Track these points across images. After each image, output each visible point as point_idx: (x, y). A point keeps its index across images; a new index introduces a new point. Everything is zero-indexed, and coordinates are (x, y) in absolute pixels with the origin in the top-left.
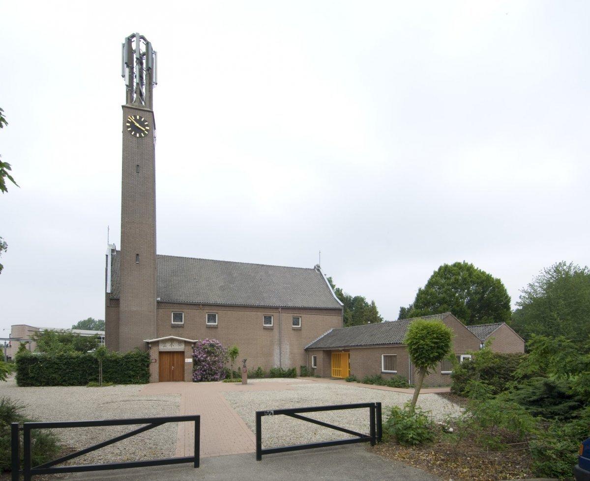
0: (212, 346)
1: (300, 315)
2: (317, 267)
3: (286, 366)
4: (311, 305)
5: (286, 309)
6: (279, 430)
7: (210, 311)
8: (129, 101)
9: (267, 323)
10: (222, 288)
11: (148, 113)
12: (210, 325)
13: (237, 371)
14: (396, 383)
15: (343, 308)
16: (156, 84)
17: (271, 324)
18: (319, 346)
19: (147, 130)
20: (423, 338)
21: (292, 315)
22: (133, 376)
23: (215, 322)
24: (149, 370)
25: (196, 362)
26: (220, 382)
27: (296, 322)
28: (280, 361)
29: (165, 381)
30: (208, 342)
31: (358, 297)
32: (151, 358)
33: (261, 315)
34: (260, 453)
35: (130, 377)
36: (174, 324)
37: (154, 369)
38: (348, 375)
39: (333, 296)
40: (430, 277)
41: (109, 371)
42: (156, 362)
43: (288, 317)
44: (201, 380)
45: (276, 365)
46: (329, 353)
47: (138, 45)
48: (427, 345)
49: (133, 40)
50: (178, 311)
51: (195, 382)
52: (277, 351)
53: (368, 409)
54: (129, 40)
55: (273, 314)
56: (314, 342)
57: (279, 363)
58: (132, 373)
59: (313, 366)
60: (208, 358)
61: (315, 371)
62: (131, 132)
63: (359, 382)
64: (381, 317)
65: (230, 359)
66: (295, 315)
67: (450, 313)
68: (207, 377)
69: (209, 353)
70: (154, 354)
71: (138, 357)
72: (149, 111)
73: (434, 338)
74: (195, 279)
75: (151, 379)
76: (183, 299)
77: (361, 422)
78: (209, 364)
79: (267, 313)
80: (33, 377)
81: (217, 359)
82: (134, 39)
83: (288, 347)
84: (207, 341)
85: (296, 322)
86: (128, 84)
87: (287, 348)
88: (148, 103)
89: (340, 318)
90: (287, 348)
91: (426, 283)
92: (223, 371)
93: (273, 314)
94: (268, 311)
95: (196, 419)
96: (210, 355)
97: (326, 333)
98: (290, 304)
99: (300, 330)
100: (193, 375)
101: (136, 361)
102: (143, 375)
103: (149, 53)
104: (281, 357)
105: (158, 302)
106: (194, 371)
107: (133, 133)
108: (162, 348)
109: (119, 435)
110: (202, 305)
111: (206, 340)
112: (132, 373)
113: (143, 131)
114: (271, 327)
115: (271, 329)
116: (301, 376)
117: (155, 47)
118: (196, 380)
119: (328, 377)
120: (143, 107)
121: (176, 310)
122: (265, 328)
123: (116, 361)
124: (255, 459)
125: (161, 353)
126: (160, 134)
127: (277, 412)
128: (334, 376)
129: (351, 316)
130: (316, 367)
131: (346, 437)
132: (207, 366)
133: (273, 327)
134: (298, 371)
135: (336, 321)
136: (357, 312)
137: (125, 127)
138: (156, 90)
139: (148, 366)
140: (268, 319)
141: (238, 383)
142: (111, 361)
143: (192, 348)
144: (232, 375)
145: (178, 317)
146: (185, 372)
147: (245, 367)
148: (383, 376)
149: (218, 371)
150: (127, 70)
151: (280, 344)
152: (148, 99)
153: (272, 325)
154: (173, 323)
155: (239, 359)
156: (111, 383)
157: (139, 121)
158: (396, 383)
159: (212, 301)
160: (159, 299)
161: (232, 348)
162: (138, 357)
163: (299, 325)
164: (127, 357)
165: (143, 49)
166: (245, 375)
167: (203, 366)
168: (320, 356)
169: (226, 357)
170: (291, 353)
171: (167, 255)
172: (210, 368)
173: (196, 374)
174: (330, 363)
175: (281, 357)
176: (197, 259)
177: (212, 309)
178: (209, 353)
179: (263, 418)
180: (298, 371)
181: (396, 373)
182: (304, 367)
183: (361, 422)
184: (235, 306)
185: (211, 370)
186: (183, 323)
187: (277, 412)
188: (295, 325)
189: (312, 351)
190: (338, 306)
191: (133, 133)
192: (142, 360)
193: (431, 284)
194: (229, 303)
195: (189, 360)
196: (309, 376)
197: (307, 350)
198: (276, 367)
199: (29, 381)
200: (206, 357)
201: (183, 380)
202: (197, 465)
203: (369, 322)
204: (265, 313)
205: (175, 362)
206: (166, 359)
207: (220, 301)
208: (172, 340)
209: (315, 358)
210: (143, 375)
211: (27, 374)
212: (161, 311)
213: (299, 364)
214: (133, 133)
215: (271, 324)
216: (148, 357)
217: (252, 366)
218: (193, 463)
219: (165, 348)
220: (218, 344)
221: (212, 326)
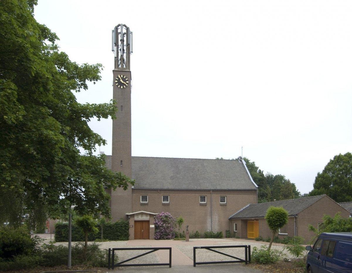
0: (166, 217)
1: (226, 195)
2: (240, 159)
3: (216, 229)
4: (234, 188)
5: (216, 191)
6: (203, 256)
7: (164, 194)
8: (116, 66)
9: (203, 201)
10: (172, 178)
11: (128, 73)
12: (165, 203)
13: (182, 233)
14: (286, 241)
15: (257, 189)
16: (132, 52)
17: (205, 201)
18: (239, 216)
19: (127, 83)
20: (272, 216)
21: (220, 195)
22: (120, 236)
23: (168, 201)
24: (128, 232)
25: (157, 227)
26: (172, 240)
27: (223, 200)
28: (211, 227)
29: (138, 239)
30: (164, 215)
31: (278, 175)
32: (130, 225)
33: (198, 196)
34: (195, 264)
35: (118, 236)
36: (142, 203)
37: (132, 231)
38: (258, 236)
39: (251, 180)
40: (327, 164)
41: (106, 233)
42: (133, 227)
43: (216, 197)
44: (160, 239)
45: (209, 230)
46: (246, 222)
47: (122, 30)
48: (274, 219)
49: (118, 28)
50: (144, 194)
51: (156, 239)
52: (209, 220)
53: (244, 248)
54: (117, 28)
55: (206, 195)
56: (235, 213)
57: (210, 228)
58: (119, 234)
59: (234, 230)
60: (164, 225)
61: (236, 233)
62: (118, 85)
63: (264, 241)
64: (298, 191)
65: (178, 225)
66: (222, 195)
67: (326, 195)
68: (163, 237)
69: (164, 222)
70: (132, 223)
71: (122, 224)
72: (128, 72)
73: (277, 216)
74: (154, 172)
75: (130, 237)
76: (147, 186)
77: (241, 254)
78: (164, 228)
79: (202, 194)
80: (65, 236)
81: (169, 225)
82: (120, 27)
83: (217, 217)
84: (163, 214)
85: (223, 200)
86: (116, 56)
87: (216, 218)
88: (127, 66)
89: (255, 196)
90: (216, 218)
91: (323, 169)
92: (173, 233)
93: (206, 195)
94: (203, 193)
95: (170, 249)
96: (165, 223)
97: (245, 207)
98: (218, 188)
99: (225, 205)
100: (155, 236)
101: (121, 226)
102: (126, 235)
103: (128, 33)
104: (212, 224)
105: (133, 189)
106: (156, 233)
107: (119, 86)
108: (136, 218)
109: (140, 254)
110: (160, 190)
111: (163, 214)
112: (119, 234)
113: (125, 85)
114: (205, 203)
115: (205, 205)
116: (226, 237)
117: (131, 30)
118: (156, 238)
119: (245, 238)
120: (125, 69)
121: (143, 194)
122: (201, 205)
123: (110, 227)
124: (193, 267)
125: (136, 222)
126: (134, 82)
127: (202, 248)
128: (249, 237)
129: (270, 192)
130: (236, 231)
131: (236, 260)
132: (164, 230)
133: (206, 203)
134: (224, 234)
135: (253, 198)
136: (274, 188)
137: (114, 83)
138: (132, 56)
139: (128, 230)
140: (203, 199)
141: (183, 241)
142: (107, 227)
143: (154, 218)
144: (179, 236)
145: (144, 198)
146: (150, 234)
147: (187, 230)
148: (279, 237)
149: (170, 233)
150: (115, 48)
151: (211, 215)
152: (127, 63)
153: (206, 202)
154: (141, 202)
155: (184, 226)
156: (108, 240)
157: (123, 79)
158: (286, 241)
159: (166, 187)
160: (133, 187)
161: (179, 219)
162: (122, 224)
163: (225, 202)
164: (116, 224)
165: (124, 31)
166: (187, 236)
167: (161, 230)
168: (239, 224)
169: (175, 224)
170: (219, 222)
171: (135, 156)
172: (164, 232)
173: (157, 235)
174: (246, 228)
175: (212, 224)
176: (155, 158)
177: (166, 192)
178: (164, 222)
179: (196, 250)
180: (224, 234)
181: (287, 235)
182: (228, 231)
183: (241, 254)
184: (181, 190)
185: (166, 232)
186: (147, 202)
187: (202, 248)
188: (222, 202)
189: (234, 220)
190: (253, 188)
191: (119, 87)
192: (125, 226)
193: (327, 169)
194: (177, 188)
195: (152, 226)
196: (231, 237)
197: (231, 220)
198: (208, 231)
199: (62, 239)
200: (163, 224)
201: (149, 238)
202: (170, 267)
203: (275, 200)
204: (201, 195)
205: (144, 228)
206: (139, 225)
207: (171, 187)
208: (142, 214)
209: (236, 225)
210: (126, 235)
211: (62, 234)
212: (134, 194)
213: (224, 228)
214: (119, 87)
215: (205, 201)
216: (128, 224)
217: (192, 230)
218: (169, 266)
219: (138, 218)
220: (170, 216)
221: (166, 204)
